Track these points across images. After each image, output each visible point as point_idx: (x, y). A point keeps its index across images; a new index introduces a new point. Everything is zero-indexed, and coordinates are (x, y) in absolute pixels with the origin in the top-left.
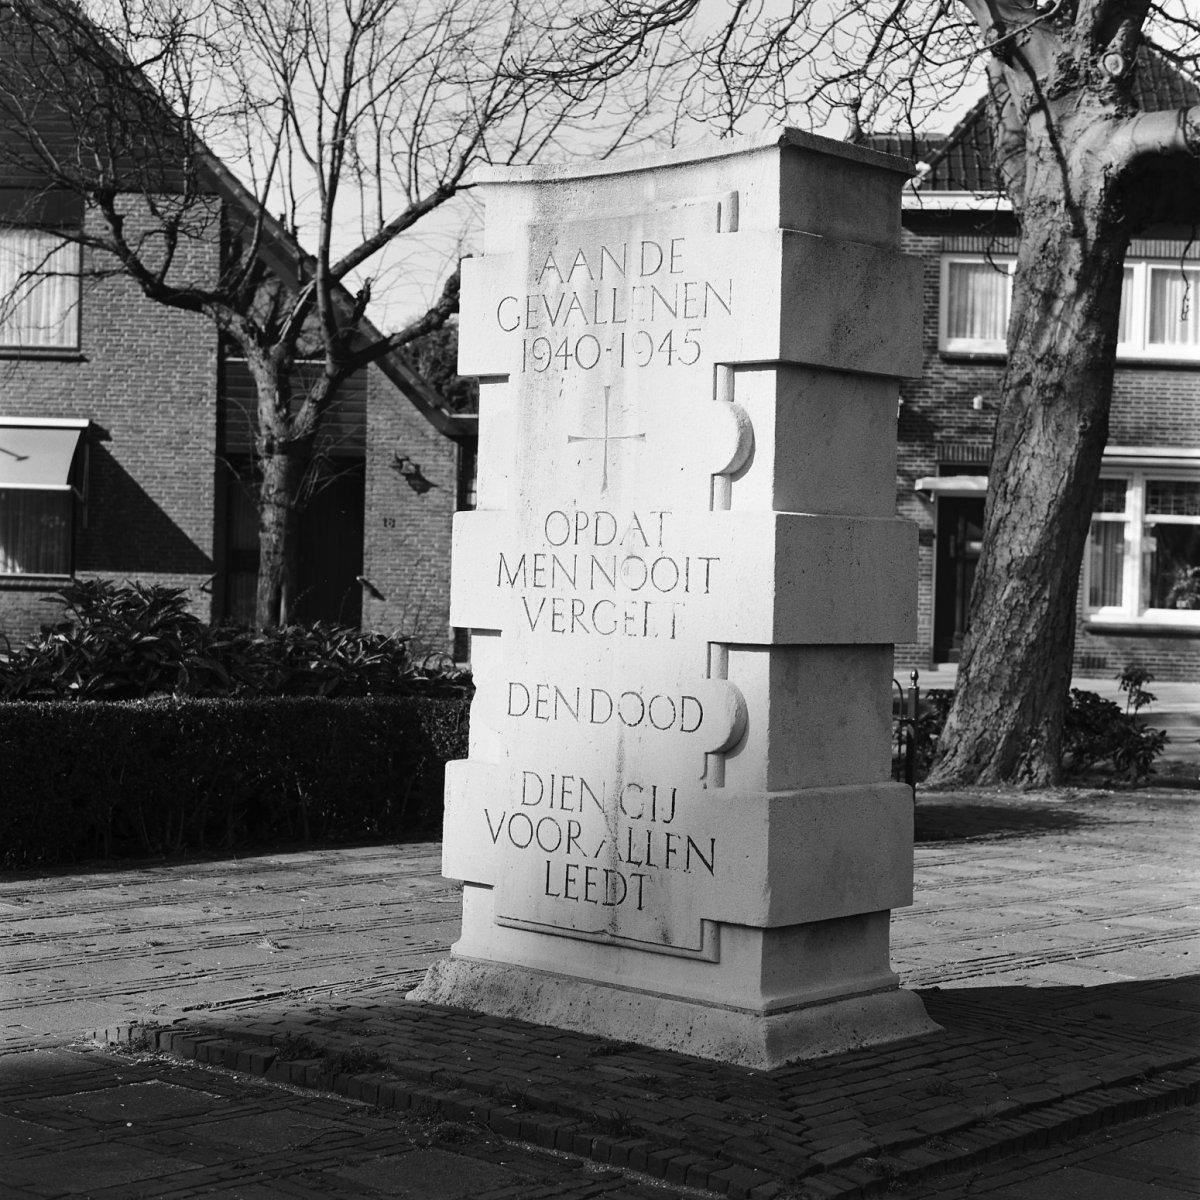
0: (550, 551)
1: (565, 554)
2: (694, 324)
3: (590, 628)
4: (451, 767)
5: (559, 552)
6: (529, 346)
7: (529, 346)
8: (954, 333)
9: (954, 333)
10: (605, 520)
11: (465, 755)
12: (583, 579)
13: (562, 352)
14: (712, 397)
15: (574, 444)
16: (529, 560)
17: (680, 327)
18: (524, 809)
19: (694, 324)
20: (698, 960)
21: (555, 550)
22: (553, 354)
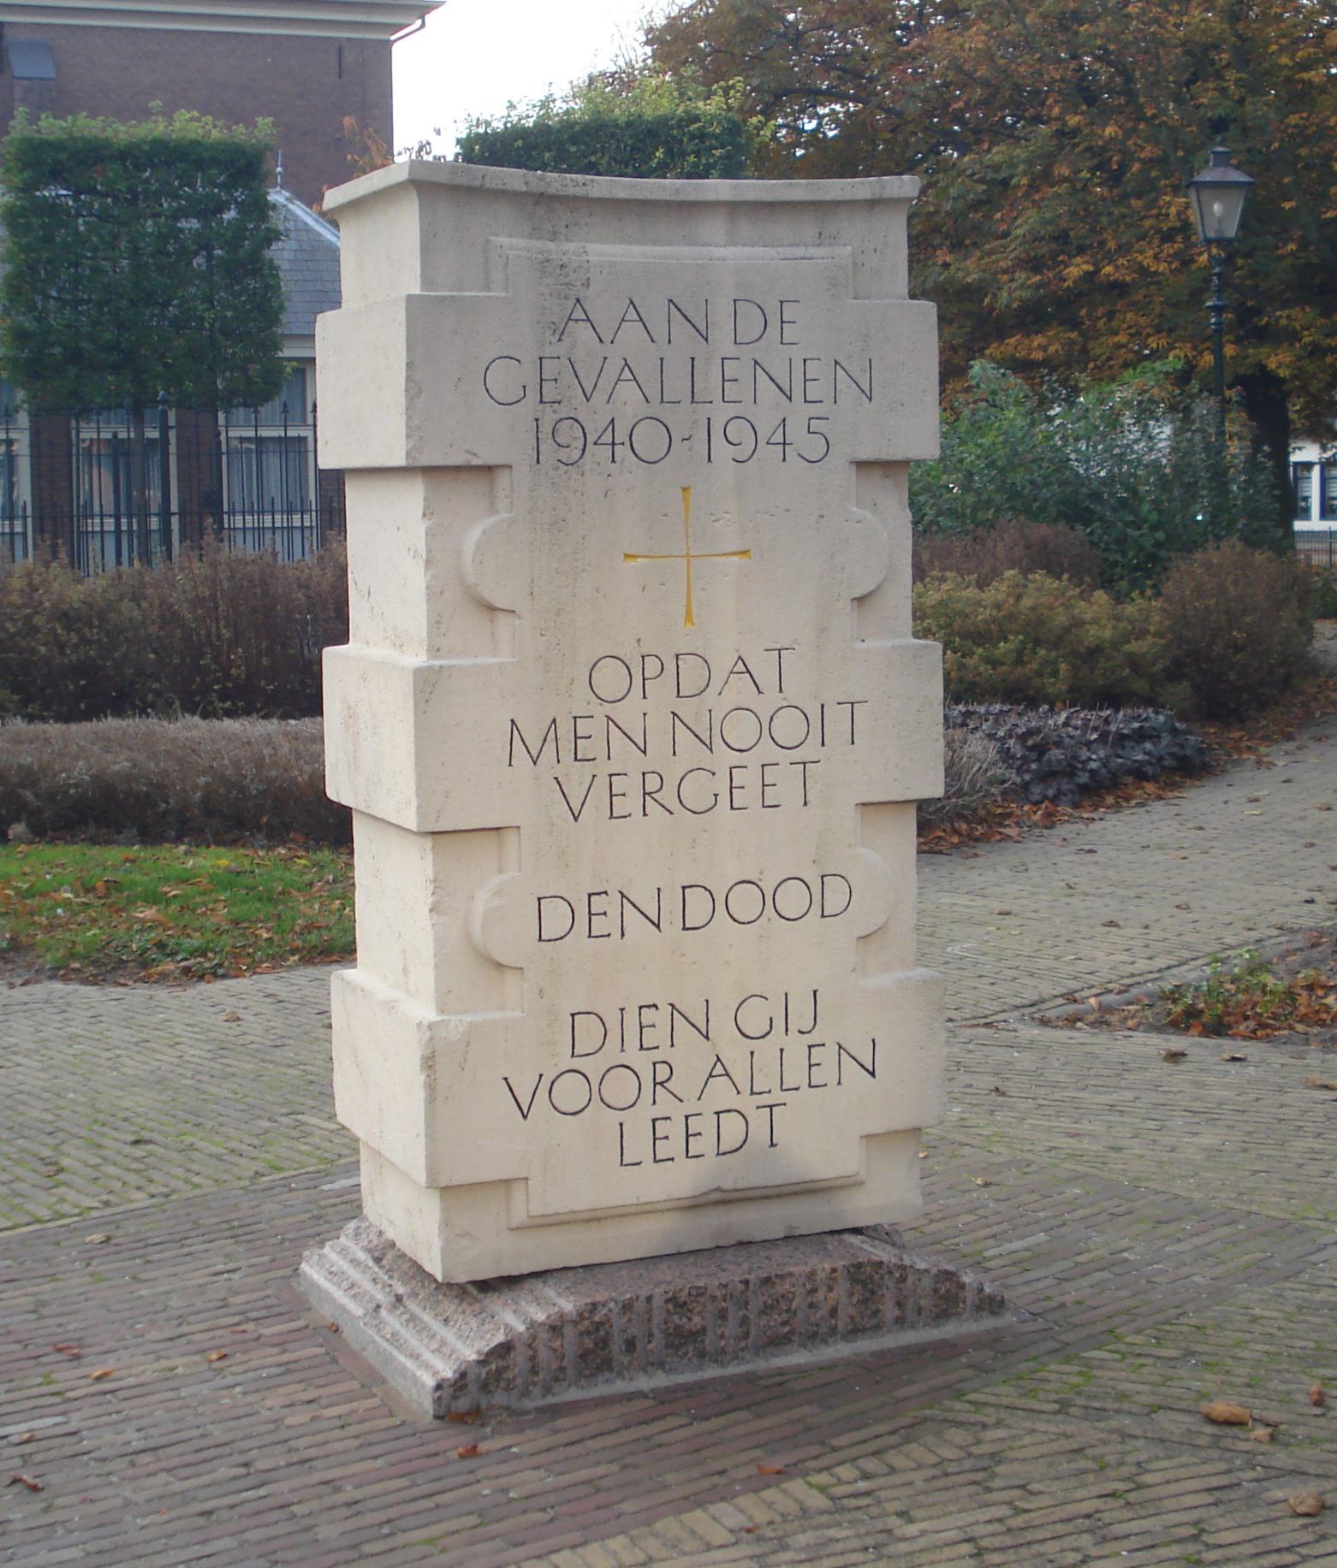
0: (600, 711)
1: (627, 713)
2: (814, 410)
3: (673, 804)
4: (330, 653)
5: (616, 711)
6: (546, 429)
7: (546, 429)
8: (1013, 592)
9: (1013, 592)
10: (687, 664)
11: (336, 303)
12: (658, 744)
13: (607, 438)
14: (866, 454)
15: (632, 563)
16: (565, 728)
17: (798, 414)
18: (576, 1063)
19: (814, 410)
20: (795, 1193)
21: (608, 709)
22: (591, 439)
